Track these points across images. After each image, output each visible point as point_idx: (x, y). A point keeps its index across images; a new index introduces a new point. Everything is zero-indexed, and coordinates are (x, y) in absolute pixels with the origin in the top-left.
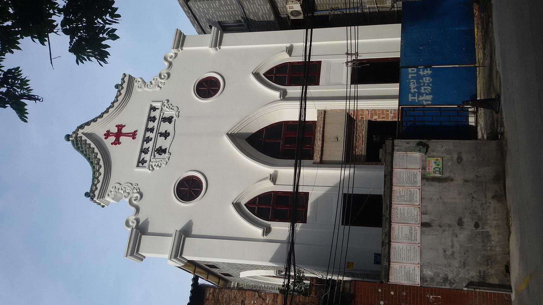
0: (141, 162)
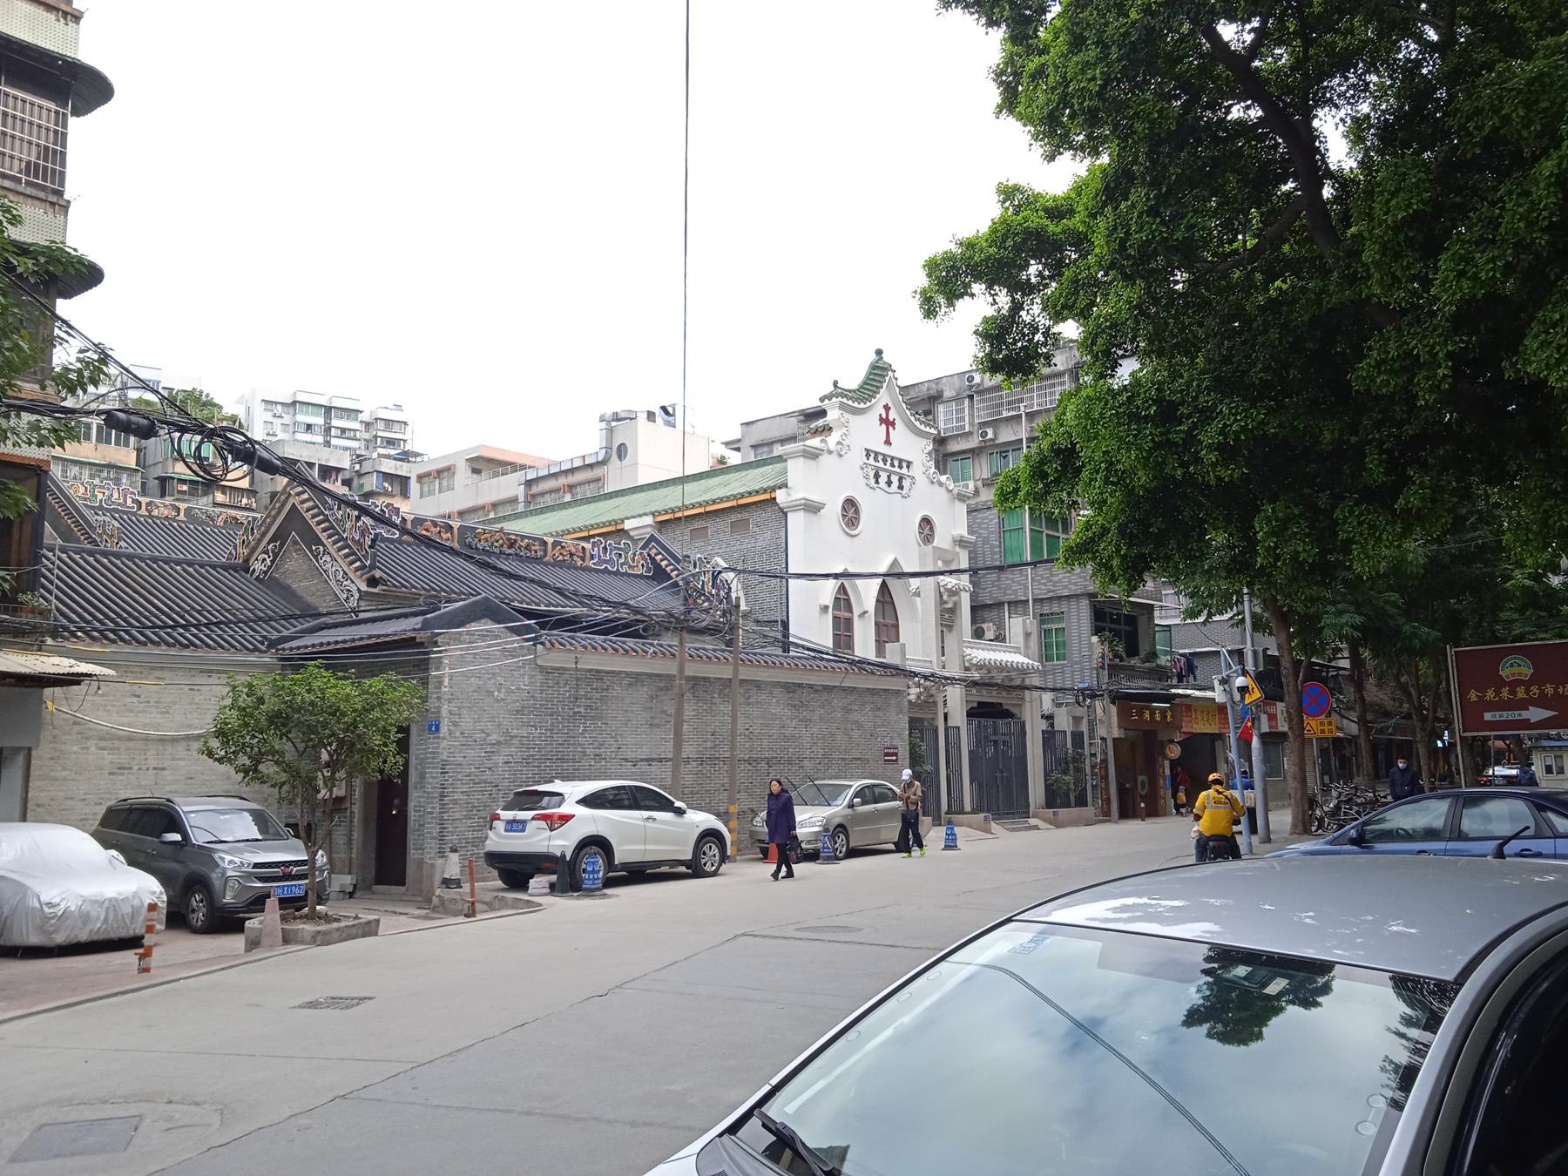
0: (868, 453)
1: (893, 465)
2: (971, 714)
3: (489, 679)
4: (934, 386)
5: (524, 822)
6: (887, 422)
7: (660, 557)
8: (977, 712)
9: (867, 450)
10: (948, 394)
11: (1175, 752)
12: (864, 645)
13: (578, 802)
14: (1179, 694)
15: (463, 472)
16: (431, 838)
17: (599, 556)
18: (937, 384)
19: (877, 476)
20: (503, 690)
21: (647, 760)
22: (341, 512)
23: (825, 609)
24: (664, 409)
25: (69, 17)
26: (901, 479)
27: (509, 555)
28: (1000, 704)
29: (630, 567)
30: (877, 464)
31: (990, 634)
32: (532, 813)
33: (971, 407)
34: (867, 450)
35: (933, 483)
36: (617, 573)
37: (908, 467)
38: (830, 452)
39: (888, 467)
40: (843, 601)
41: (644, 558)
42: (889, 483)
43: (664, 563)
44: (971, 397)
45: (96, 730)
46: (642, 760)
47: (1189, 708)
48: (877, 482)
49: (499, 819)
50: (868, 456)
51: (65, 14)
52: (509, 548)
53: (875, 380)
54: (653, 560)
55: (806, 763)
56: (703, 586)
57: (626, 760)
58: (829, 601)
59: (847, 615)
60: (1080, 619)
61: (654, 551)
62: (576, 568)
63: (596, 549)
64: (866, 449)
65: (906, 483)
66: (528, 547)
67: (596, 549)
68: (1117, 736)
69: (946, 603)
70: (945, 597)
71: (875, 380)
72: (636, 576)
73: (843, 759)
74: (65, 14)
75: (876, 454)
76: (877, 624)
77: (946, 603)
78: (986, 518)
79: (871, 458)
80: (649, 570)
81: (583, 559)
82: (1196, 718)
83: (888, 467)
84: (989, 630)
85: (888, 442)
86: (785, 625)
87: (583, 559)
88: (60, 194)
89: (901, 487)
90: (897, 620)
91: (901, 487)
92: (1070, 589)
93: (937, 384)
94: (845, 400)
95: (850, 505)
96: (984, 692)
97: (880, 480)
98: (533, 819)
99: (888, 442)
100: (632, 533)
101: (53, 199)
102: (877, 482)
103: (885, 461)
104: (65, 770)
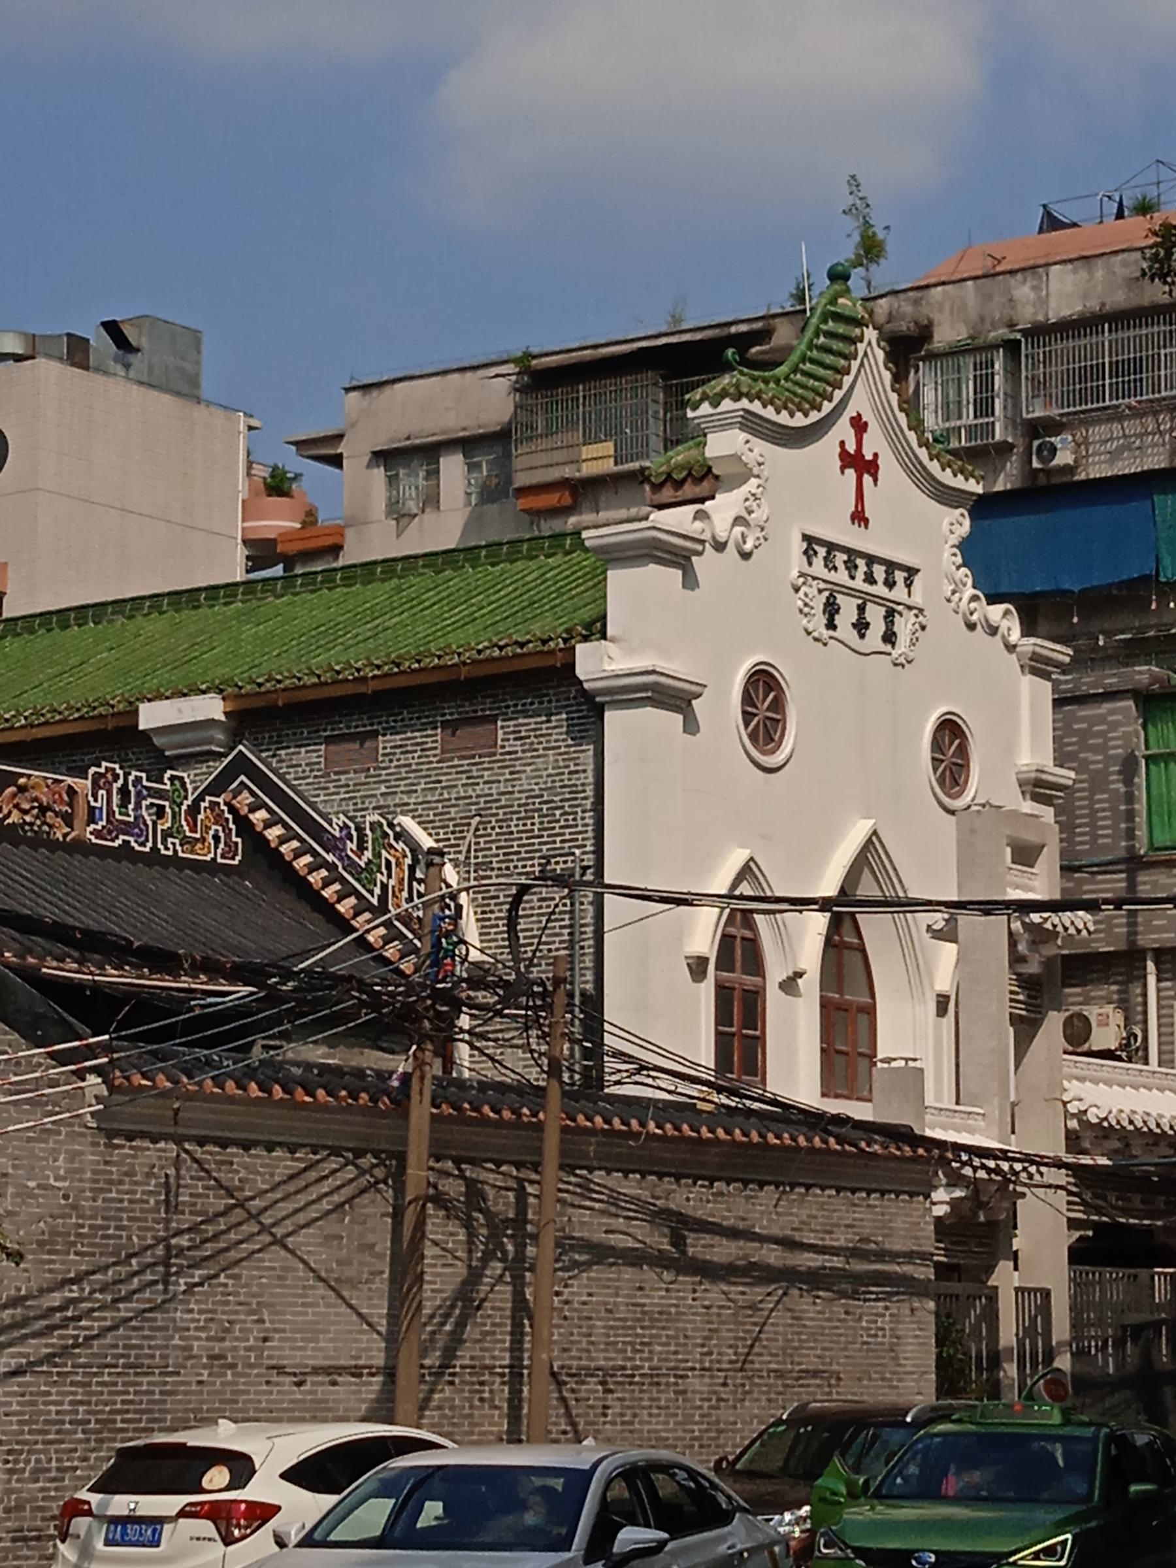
1: (870, 579)
2: (1077, 1255)
4: (908, 309)
5: (157, 1521)
7: (262, 814)
10: (946, 334)
13: (285, 1476)
17: (111, 812)
18: (916, 302)
19: (831, 609)
21: (327, 1371)
23: (698, 967)
24: (112, 328)
26: (890, 615)
29: (185, 841)
31: (1106, 1036)
32: (182, 1500)
33: (1013, 373)
35: (971, 627)
38: (720, 547)
39: (859, 583)
41: (219, 819)
42: (861, 626)
43: (274, 833)
44: (1012, 348)
46: (316, 1370)
48: (831, 626)
50: (809, 554)
53: (828, 350)
54: (244, 825)
55: (694, 1383)
56: (383, 898)
57: (280, 1370)
59: (750, 980)
61: (245, 798)
62: (54, 846)
65: (904, 626)
67: (102, 792)
70: (1022, 948)
71: (828, 350)
72: (197, 866)
73: (780, 1374)
75: (831, 547)
76: (825, 1004)
78: (1102, 719)
79: (818, 562)
81: (68, 820)
83: (859, 583)
85: (859, 517)
87: (68, 820)
89: (889, 637)
90: (873, 996)
91: (889, 637)
93: (916, 302)
94: (756, 407)
97: (838, 620)
98: (183, 1514)
99: (859, 517)
100: (157, 741)
102: (831, 626)
103: (851, 567)
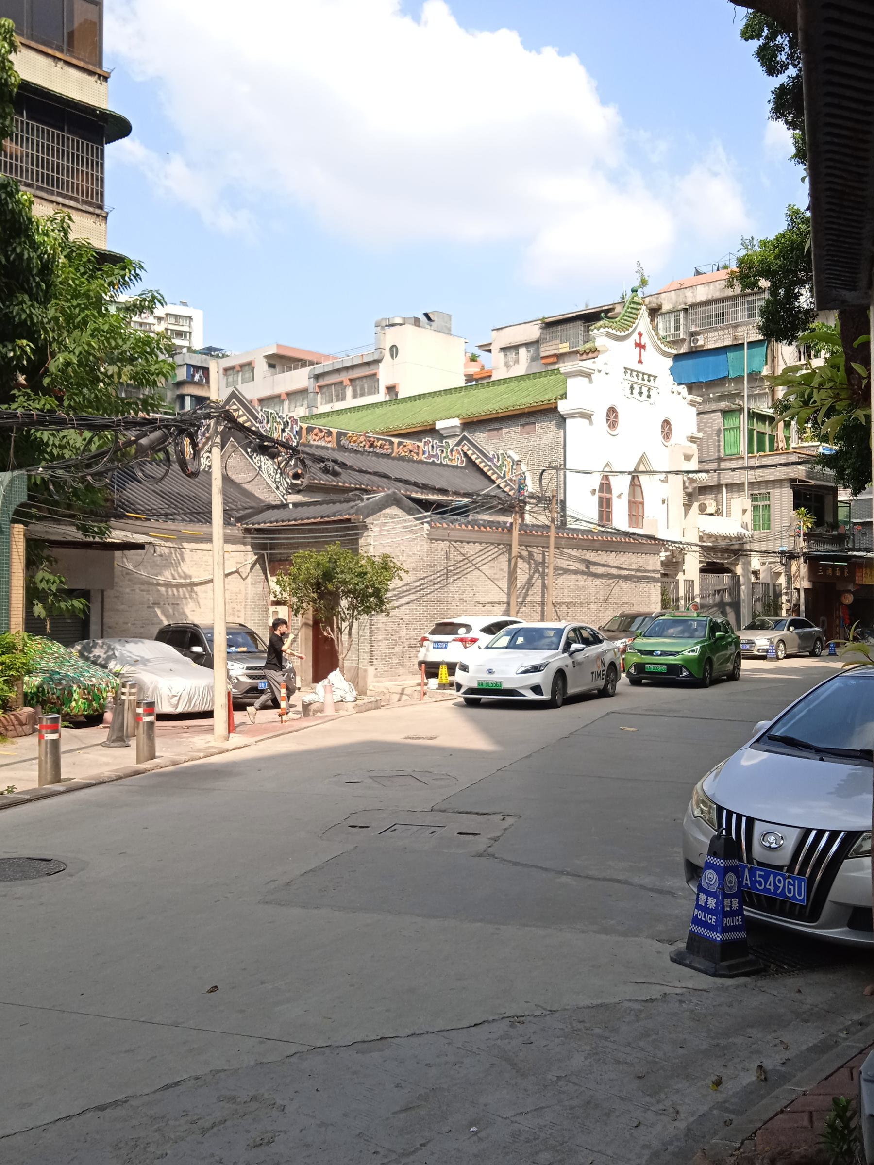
1: (643, 379)
3: (397, 547)
5: (446, 642)
6: (640, 346)
8: (709, 569)
9: (625, 368)
10: (666, 308)
11: (849, 599)
12: (620, 520)
14: (855, 556)
15: (261, 366)
16: (364, 652)
17: (429, 452)
18: (657, 298)
19: (632, 388)
20: (405, 555)
21: (492, 603)
22: (269, 425)
25: (102, 78)
26: (649, 390)
27: (369, 452)
28: (723, 564)
29: (450, 460)
30: (632, 379)
31: (711, 509)
33: (686, 318)
34: (625, 368)
36: (441, 465)
37: (654, 380)
39: (640, 381)
40: (605, 487)
41: (459, 453)
42: (641, 393)
45: (139, 578)
46: (488, 603)
47: (861, 566)
48: (632, 393)
49: (428, 640)
50: (626, 373)
51: (100, 76)
52: (370, 447)
53: (631, 313)
54: (465, 454)
56: (504, 475)
57: (479, 603)
58: (597, 487)
60: (784, 497)
62: (414, 461)
63: (426, 447)
64: (625, 368)
66: (381, 447)
67: (426, 447)
68: (807, 587)
69: (687, 488)
70: (687, 484)
72: (453, 467)
73: (616, 604)
74: (100, 76)
76: (630, 502)
77: (687, 488)
78: (711, 418)
79: (628, 375)
80: (462, 462)
81: (417, 454)
82: (866, 573)
83: (640, 381)
84: (711, 505)
85: (640, 361)
86: (563, 503)
87: (417, 454)
88: (101, 207)
89: (649, 396)
91: (649, 396)
92: (775, 475)
94: (610, 330)
95: (612, 410)
96: (712, 554)
97: (634, 391)
98: (454, 640)
99: (640, 361)
100: (441, 432)
101: (98, 211)
102: (632, 393)
103: (638, 376)
104: (123, 604)
